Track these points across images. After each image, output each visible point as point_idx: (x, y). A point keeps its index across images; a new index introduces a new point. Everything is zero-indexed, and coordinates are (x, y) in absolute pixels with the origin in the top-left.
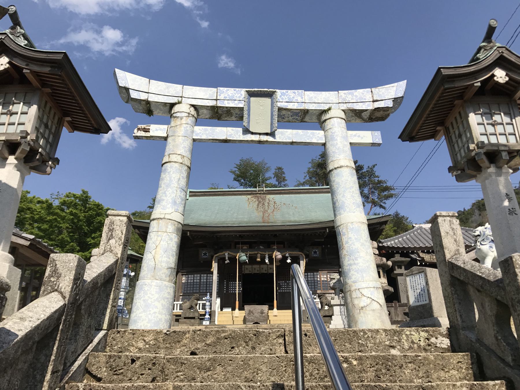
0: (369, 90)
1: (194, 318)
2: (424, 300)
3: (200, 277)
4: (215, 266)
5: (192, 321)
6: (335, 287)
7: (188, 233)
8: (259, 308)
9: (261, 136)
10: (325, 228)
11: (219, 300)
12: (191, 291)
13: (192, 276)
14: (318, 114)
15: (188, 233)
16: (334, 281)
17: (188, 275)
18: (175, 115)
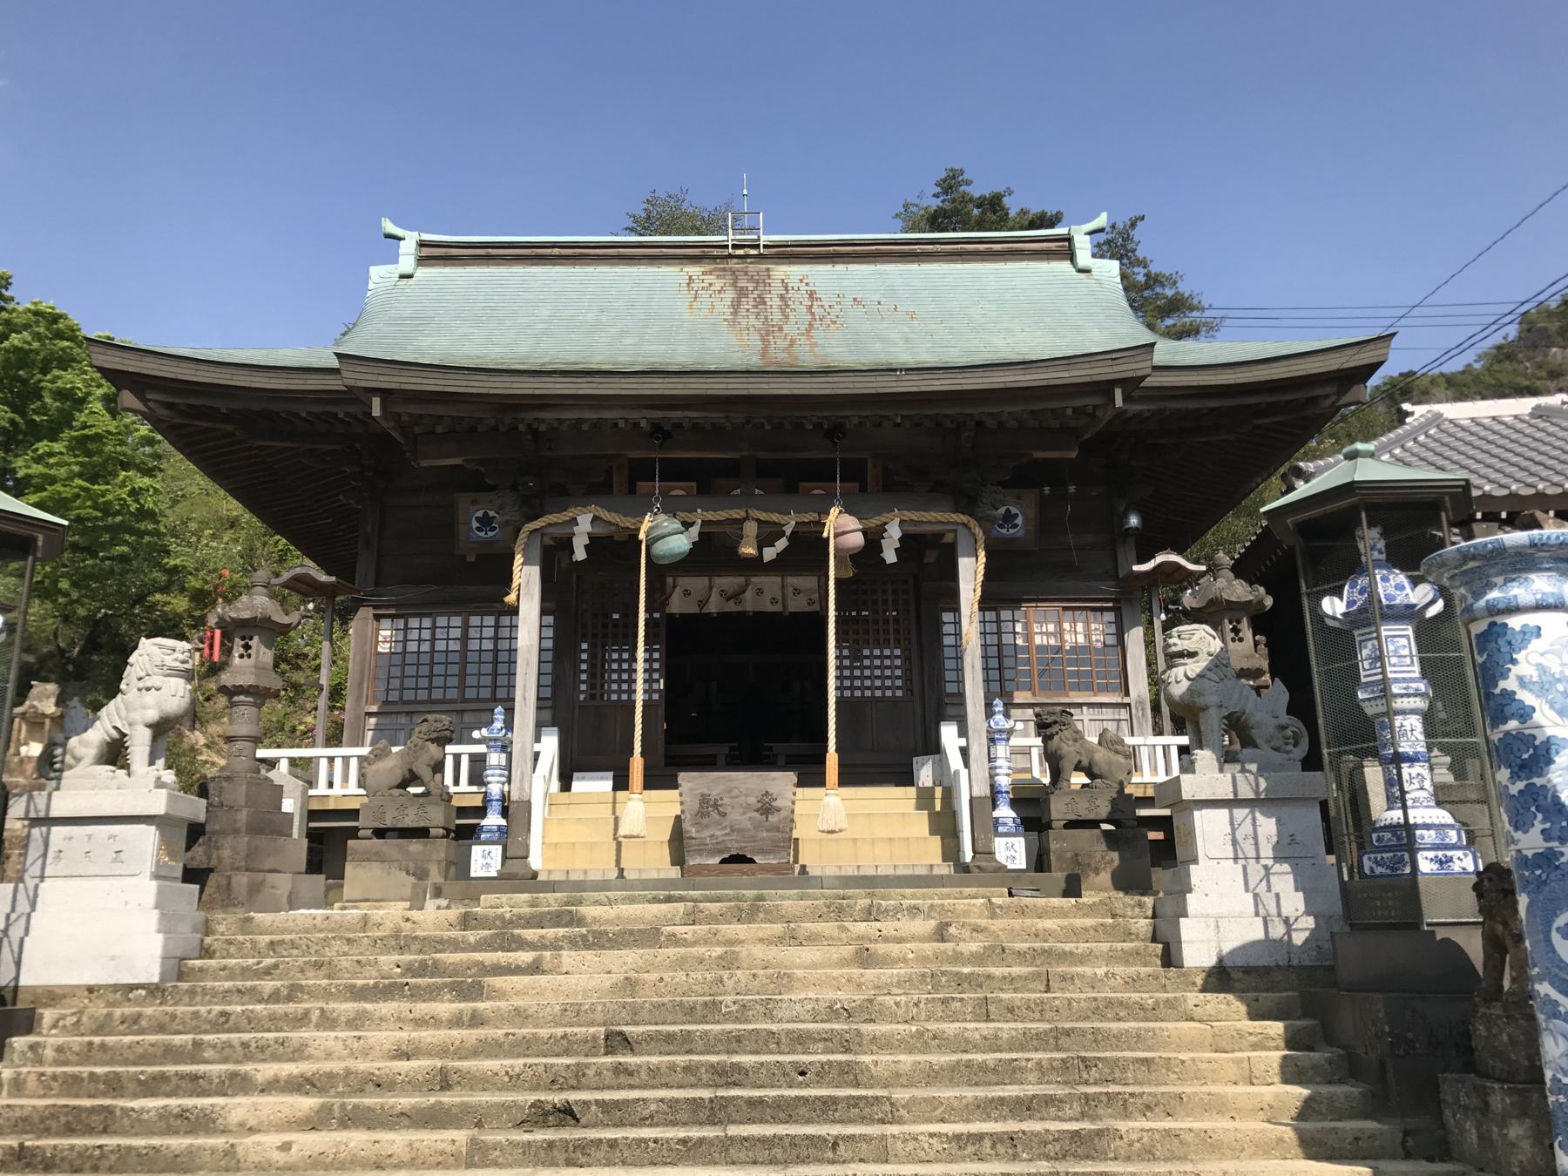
1: (422, 833)
2: (338, 763)
3: (466, 628)
4: (526, 580)
5: (415, 846)
6: (1200, 701)
7: (376, 403)
8: (746, 784)
10: (1104, 388)
11: (550, 744)
12: (422, 695)
13: (427, 622)
15: (376, 403)
16: (1194, 667)
17: (405, 617)
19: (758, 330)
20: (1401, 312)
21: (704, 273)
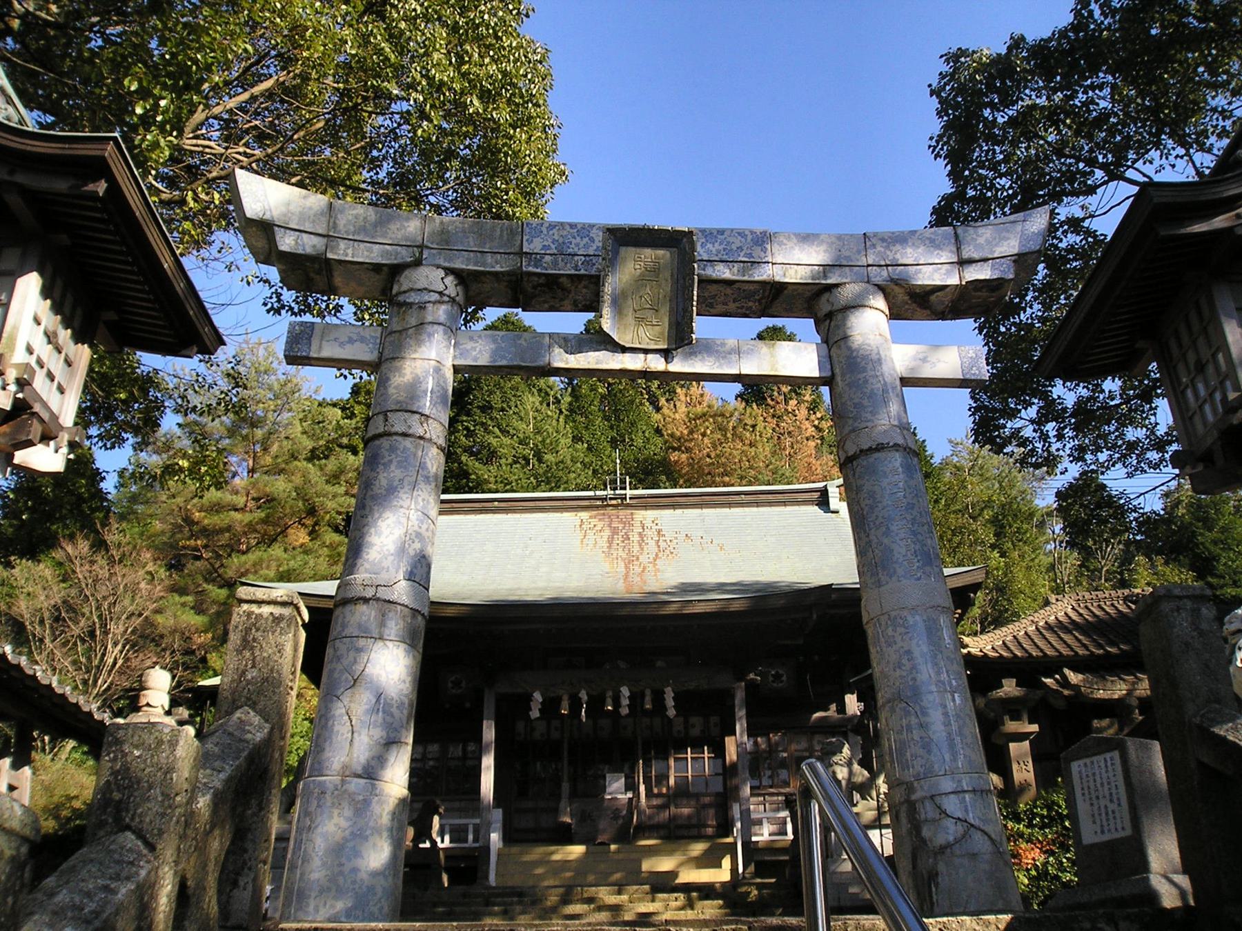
2: (1119, 827)
9: (650, 356)
14: (808, 294)
18: (401, 298)
19: (624, 560)
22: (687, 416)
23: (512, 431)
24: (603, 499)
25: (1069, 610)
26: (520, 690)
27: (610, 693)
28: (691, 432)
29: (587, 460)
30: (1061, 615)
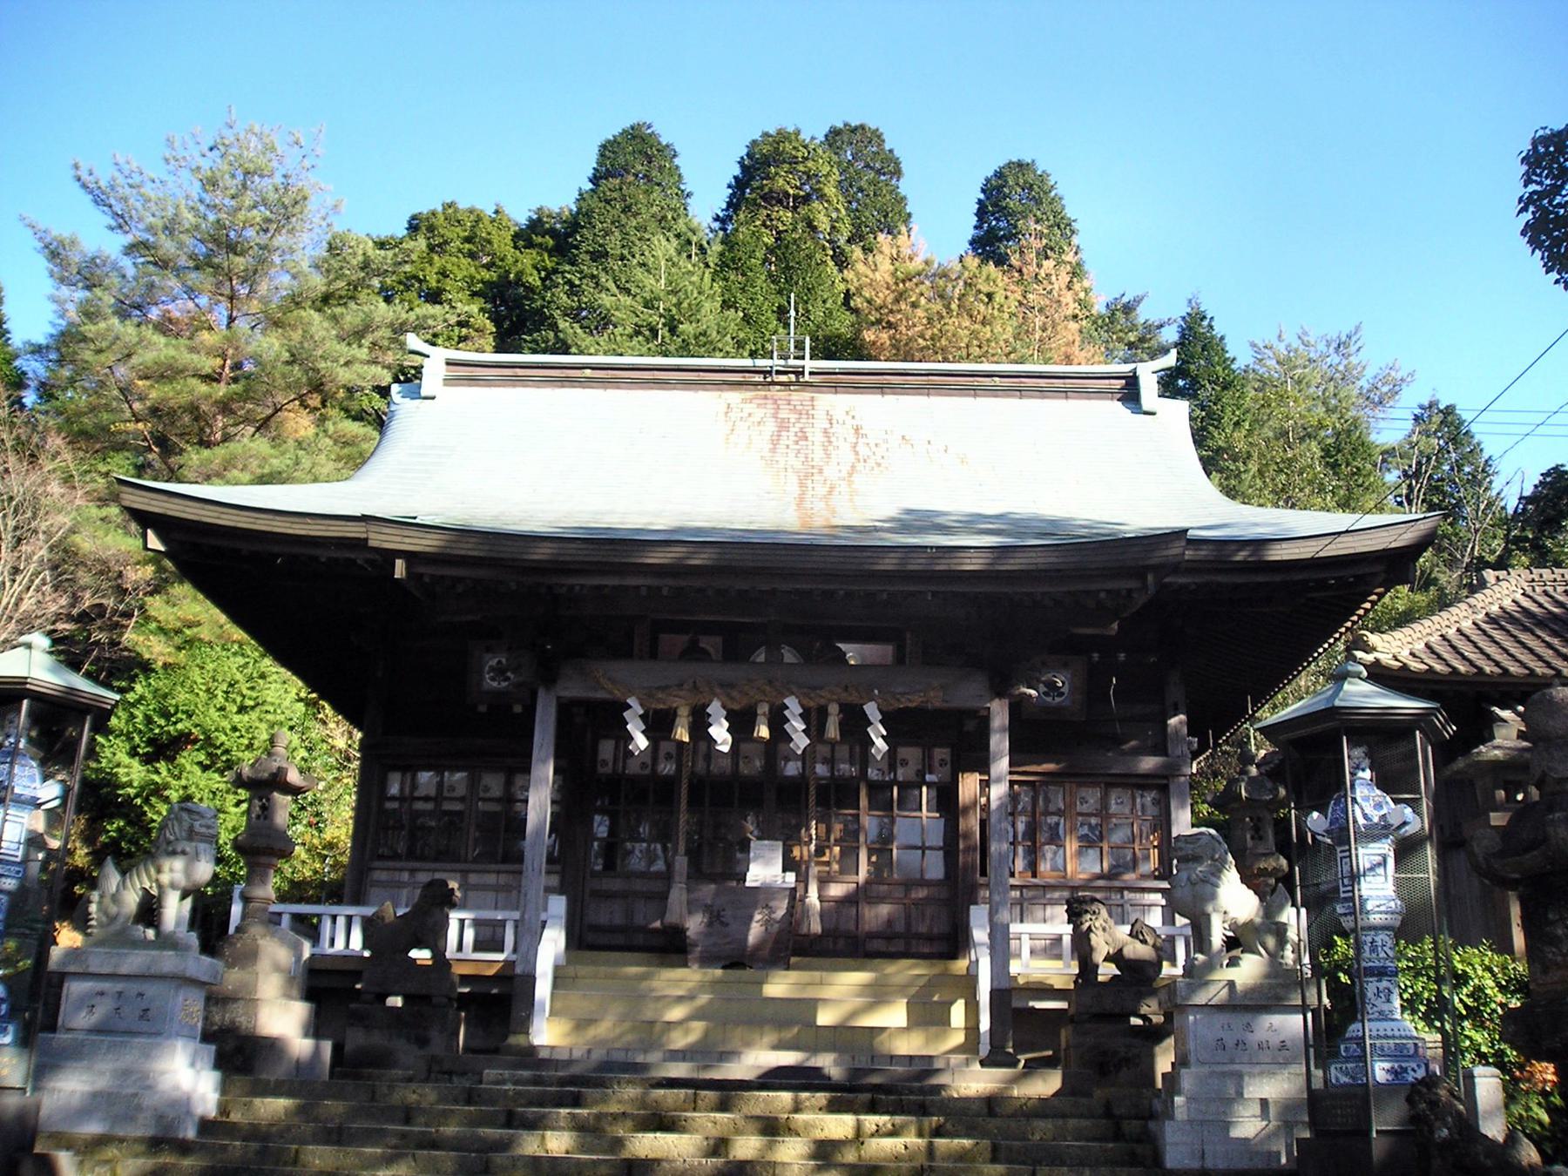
0: (1209, 1164)
2: (341, 921)
20: (1541, 430)
21: (744, 401)
22: (893, 274)
23: (634, 290)
24: (766, 373)
25: (1519, 597)
26: (601, 695)
27: (763, 709)
28: (897, 301)
29: (742, 335)
30: (1507, 603)
